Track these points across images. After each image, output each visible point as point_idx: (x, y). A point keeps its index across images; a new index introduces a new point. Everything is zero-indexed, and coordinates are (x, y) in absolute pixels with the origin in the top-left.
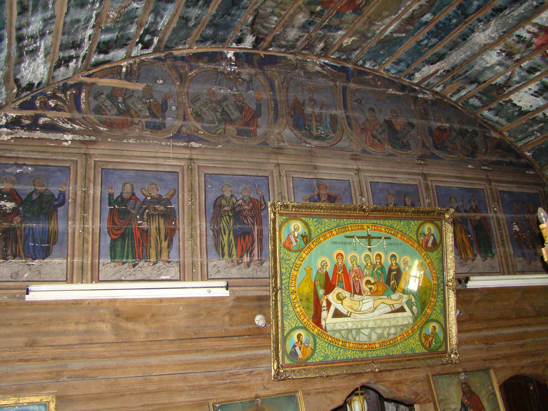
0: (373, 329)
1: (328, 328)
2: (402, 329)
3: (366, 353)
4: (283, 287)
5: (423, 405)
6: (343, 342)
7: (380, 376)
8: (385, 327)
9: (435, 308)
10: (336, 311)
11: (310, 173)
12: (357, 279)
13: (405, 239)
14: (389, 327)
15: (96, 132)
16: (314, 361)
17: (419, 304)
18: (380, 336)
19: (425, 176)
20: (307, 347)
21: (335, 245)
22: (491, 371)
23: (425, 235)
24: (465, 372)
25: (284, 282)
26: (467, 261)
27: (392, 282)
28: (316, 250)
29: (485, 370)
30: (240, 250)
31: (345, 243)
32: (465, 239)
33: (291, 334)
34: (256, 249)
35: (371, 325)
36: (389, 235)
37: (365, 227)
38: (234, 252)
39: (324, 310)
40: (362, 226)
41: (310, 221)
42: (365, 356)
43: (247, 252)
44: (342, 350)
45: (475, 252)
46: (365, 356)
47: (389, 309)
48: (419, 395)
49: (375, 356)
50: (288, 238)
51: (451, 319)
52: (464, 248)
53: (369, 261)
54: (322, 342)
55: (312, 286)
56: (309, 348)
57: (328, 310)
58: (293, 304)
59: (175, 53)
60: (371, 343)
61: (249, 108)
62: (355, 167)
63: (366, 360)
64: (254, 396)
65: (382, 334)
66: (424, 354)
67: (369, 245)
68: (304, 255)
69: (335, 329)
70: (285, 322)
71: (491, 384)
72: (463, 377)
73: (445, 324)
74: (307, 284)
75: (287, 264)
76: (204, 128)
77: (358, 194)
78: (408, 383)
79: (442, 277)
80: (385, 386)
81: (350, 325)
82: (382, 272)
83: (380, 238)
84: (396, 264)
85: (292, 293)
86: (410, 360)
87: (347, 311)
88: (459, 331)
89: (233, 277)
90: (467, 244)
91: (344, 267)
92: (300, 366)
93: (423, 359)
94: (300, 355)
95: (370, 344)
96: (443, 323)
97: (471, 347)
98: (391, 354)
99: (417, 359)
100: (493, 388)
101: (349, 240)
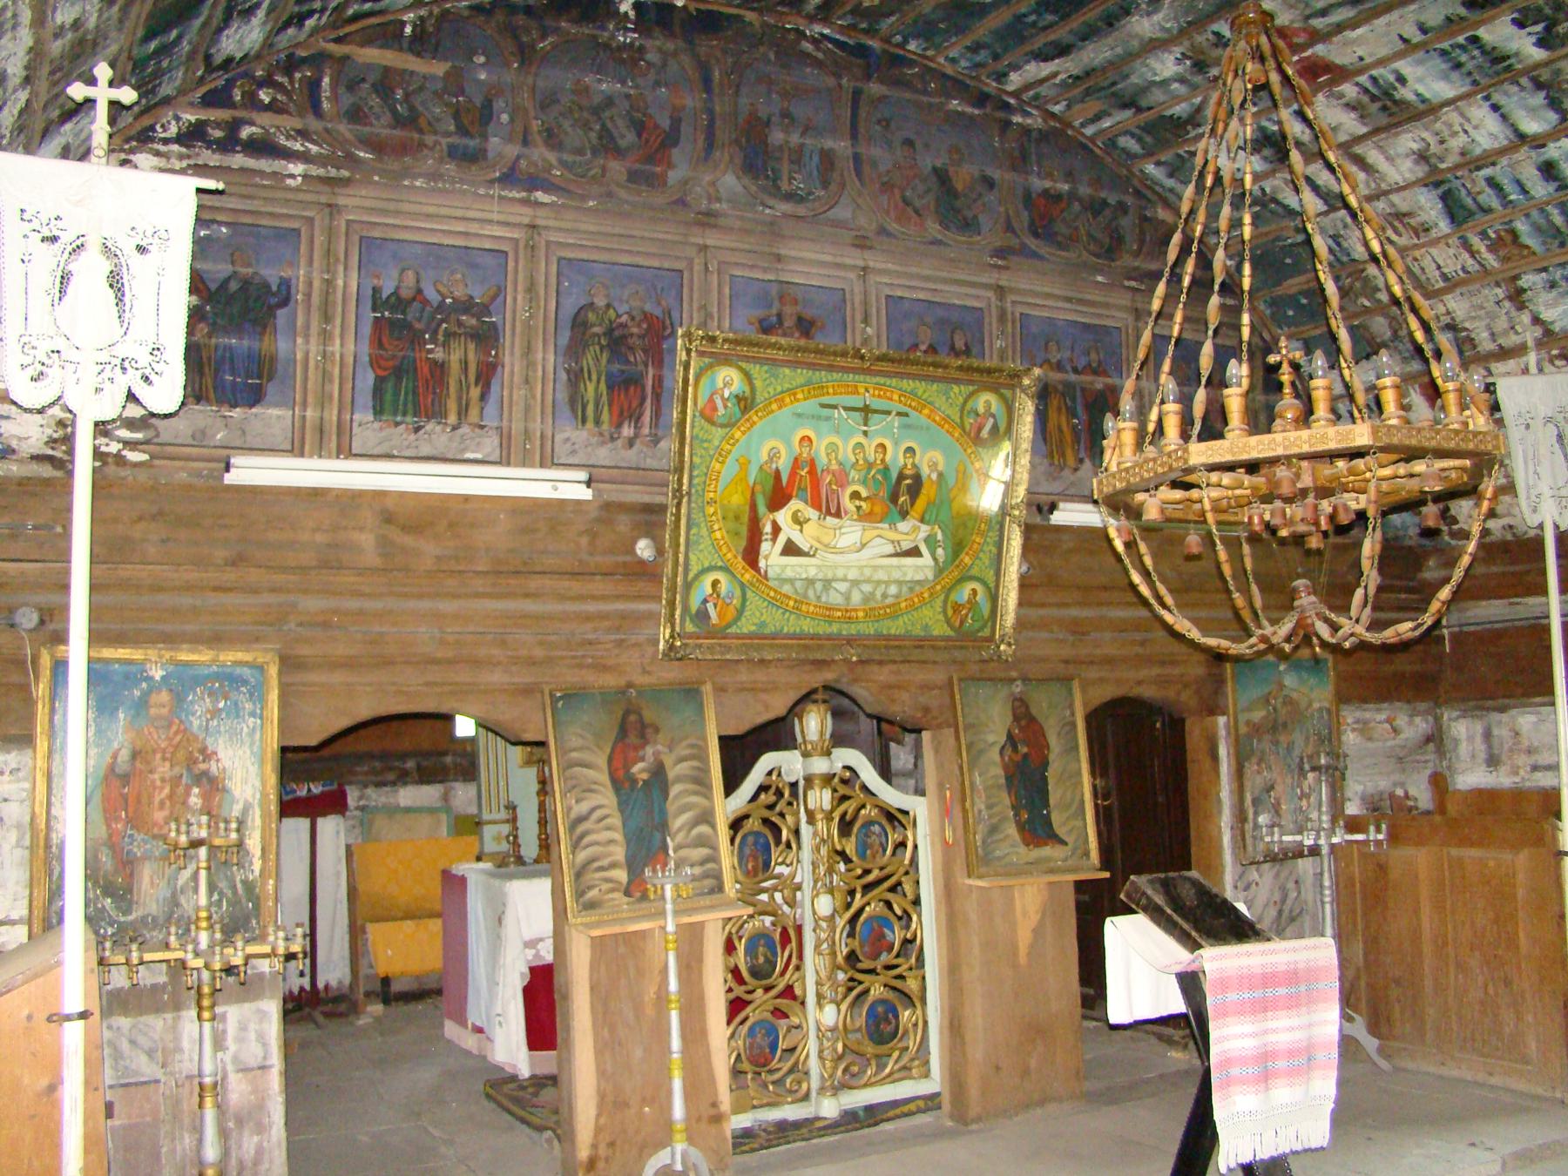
1: (771, 574)
2: (911, 589)
8: (879, 582)
11: (765, 270)
14: (887, 583)
15: (351, 160)
18: (867, 598)
19: (1001, 291)
22: (1076, 684)
25: (696, 481)
30: (615, 418)
31: (819, 418)
32: (1065, 428)
37: (862, 390)
38: (605, 416)
41: (755, 370)
47: (890, 549)
50: (711, 400)
57: (774, 539)
61: (656, 126)
62: (861, 263)
65: (872, 594)
66: (948, 639)
70: (692, 557)
72: (1018, 688)
73: (997, 587)
76: (563, 164)
77: (859, 317)
81: (812, 572)
84: (914, 465)
90: (1068, 436)
91: (812, 463)
96: (992, 585)
97: (1044, 635)
100: (1073, 714)
101: (826, 412)
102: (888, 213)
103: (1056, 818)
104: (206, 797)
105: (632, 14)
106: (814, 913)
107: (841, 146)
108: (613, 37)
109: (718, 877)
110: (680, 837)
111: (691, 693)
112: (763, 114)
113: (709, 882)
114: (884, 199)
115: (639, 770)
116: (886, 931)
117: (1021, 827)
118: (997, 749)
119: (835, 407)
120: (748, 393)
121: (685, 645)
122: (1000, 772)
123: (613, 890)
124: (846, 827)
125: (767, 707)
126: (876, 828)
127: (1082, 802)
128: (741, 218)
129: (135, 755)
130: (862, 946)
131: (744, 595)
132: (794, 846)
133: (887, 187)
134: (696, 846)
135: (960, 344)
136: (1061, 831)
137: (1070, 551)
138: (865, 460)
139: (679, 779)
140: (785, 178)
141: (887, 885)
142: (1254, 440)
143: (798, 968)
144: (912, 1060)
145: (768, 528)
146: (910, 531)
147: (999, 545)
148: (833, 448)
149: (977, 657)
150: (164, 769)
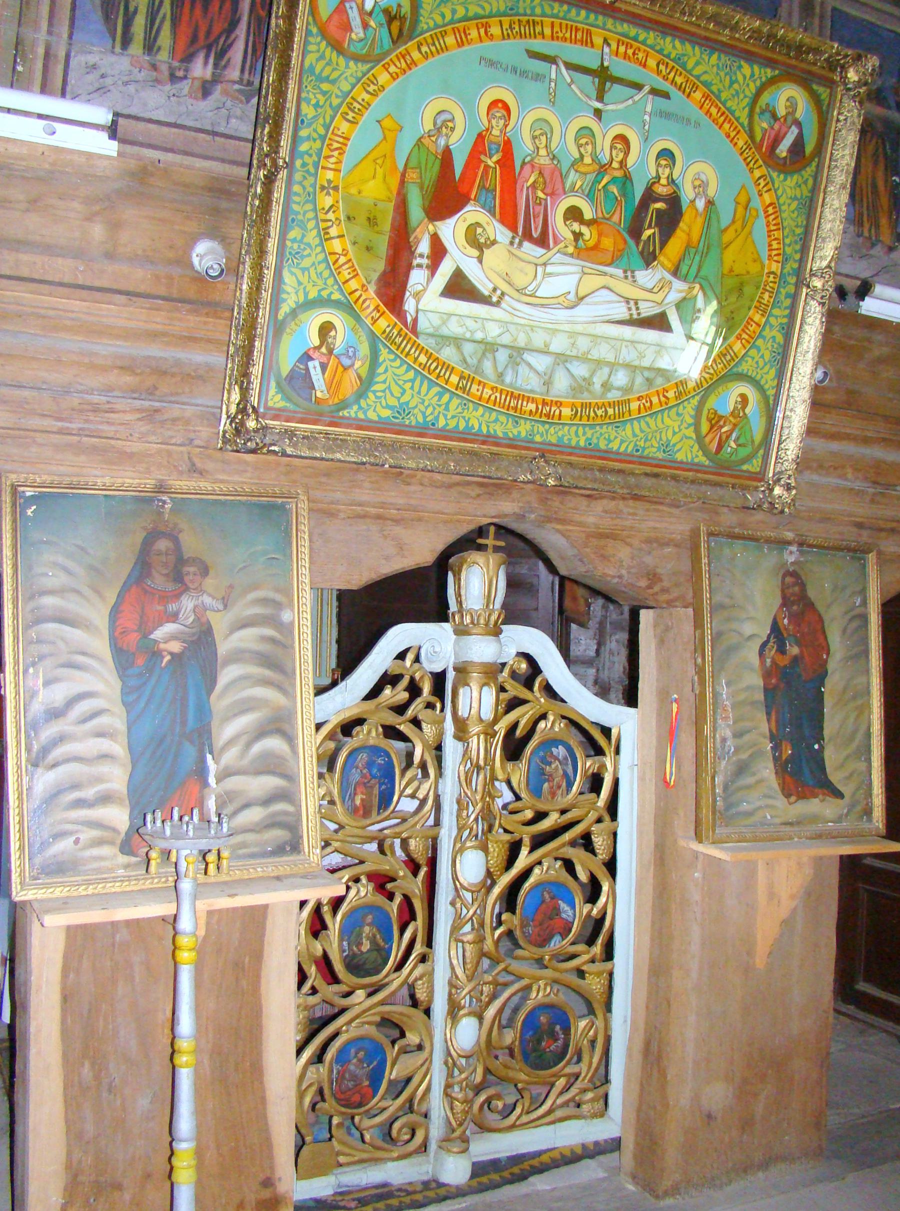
0: (562, 359)
1: (422, 325)
2: (649, 381)
3: (528, 426)
4: (298, 163)
5: (666, 613)
6: (462, 378)
7: (557, 504)
8: (599, 363)
9: (759, 342)
12: (540, 194)
13: (714, 111)
14: (613, 366)
16: (361, 415)
18: (580, 386)
20: (345, 369)
21: (491, 70)
22: (872, 557)
23: (774, 116)
24: (801, 544)
25: (303, 147)
26: (873, 245)
27: (648, 233)
29: (854, 550)
30: (183, 42)
31: (524, 74)
32: (881, 184)
33: (302, 317)
34: (240, 46)
35: (559, 344)
36: (666, 86)
37: (598, 41)
38: (165, 39)
39: (420, 266)
40: (589, 33)
42: (523, 434)
43: (209, 48)
44: (456, 401)
46: (523, 434)
47: (621, 311)
48: (661, 580)
49: (554, 440)
51: (796, 385)
52: (874, 208)
53: (589, 148)
54: (398, 362)
55: (394, 183)
56: (352, 374)
58: (322, 225)
60: (548, 399)
63: (525, 448)
64: (150, 483)
65: (588, 381)
66: (695, 468)
67: (600, 99)
68: (384, 78)
69: (445, 331)
70: (287, 277)
71: (863, 592)
72: (791, 556)
73: (777, 396)
74: (380, 172)
75: (324, 93)
78: (636, 542)
79: (797, 257)
80: (567, 538)
81: (493, 332)
82: (624, 195)
83: (638, 87)
84: (672, 181)
85: (323, 188)
86: (656, 476)
87: (491, 286)
88: (811, 431)
89: (147, 115)
91: (507, 148)
92: (315, 422)
93: (693, 482)
95: (544, 403)
96: (771, 392)
97: (833, 481)
98: (602, 446)
99: (675, 478)
100: (864, 603)
103: (831, 757)
106: (455, 878)
109: (293, 827)
110: (230, 757)
111: (271, 512)
113: (279, 834)
116: (563, 906)
117: (782, 768)
118: (757, 643)
120: (406, 9)
121: (265, 428)
122: (756, 680)
123: (99, 842)
124: (514, 748)
125: (401, 548)
126: (561, 751)
127: (868, 735)
130: (523, 926)
132: (432, 771)
134: (258, 773)
136: (835, 777)
137: (881, 361)
139: (237, 656)
141: (567, 836)
143: (423, 959)
144: (584, 1091)
146: (653, 286)
147: (788, 331)
149: (739, 503)
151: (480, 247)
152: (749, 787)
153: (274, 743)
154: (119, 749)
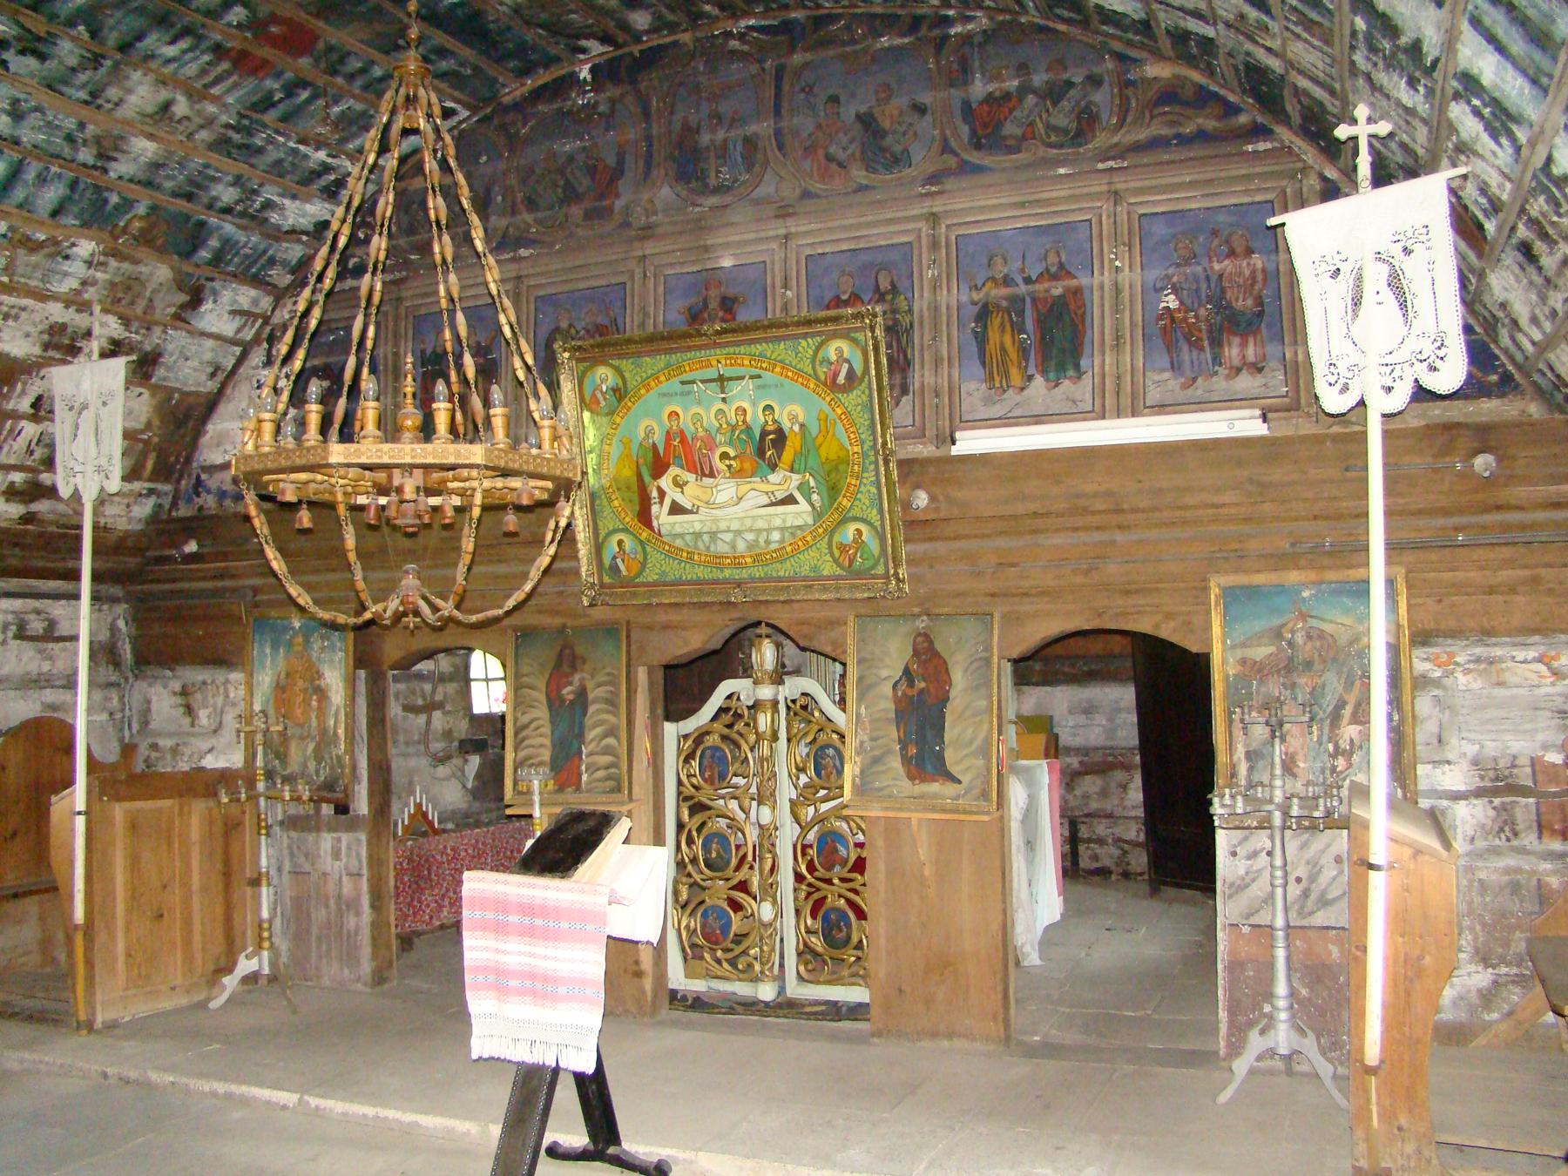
0: (738, 533)
8: (760, 531)
10: (674, 503)
11: (694, 262)
14: (769, 531)
15: (407, 262)
17: (824, 490)
18: (751, 546)
19: (934, 218)
28: (637, 408)
35: (735, 526)
36: (757, 372)
41: (626, 365)
45: (1032, 370)
47: (765, 500)
50: (594, 395)
55: (634, 467)
57: (661, 503)
59: (507, 100)
61: (606, 167)
62: (782, 231)
65: (756, 541)
72: (921, 624)
76: (538, 222)
77: (778, 283)
81: (698, 527)
84: (775, 421)
90: (1013, 354)
94: (624, 571)
101: (688, 387)
102: (811, 177)
103: (950, 756)
104: (319, 701)
105: (589, 78)
107: (763, 128)
108: (575, 101)
110: (591, 747)
112: (693, 123)
113: (612, 783)
114: (807, 165)
115: (568, 692)
116: (840, 847)
117: (906, 760)
119: (693, 382)
126: (831, 751)
128: (674, 223)
129: (288, 675)
131: (644, 549)
133: (809, 151)
135: (884, 284)
138: (728, 423)
140: (713, 174)
142: (386, 447)
145: (655, 494)
146: (781, 481)
148: (697, 418)
150: (300, 684)
151: (681, 486)
152: (883, 772)
153: (611, 741)
154: (547, 742)
